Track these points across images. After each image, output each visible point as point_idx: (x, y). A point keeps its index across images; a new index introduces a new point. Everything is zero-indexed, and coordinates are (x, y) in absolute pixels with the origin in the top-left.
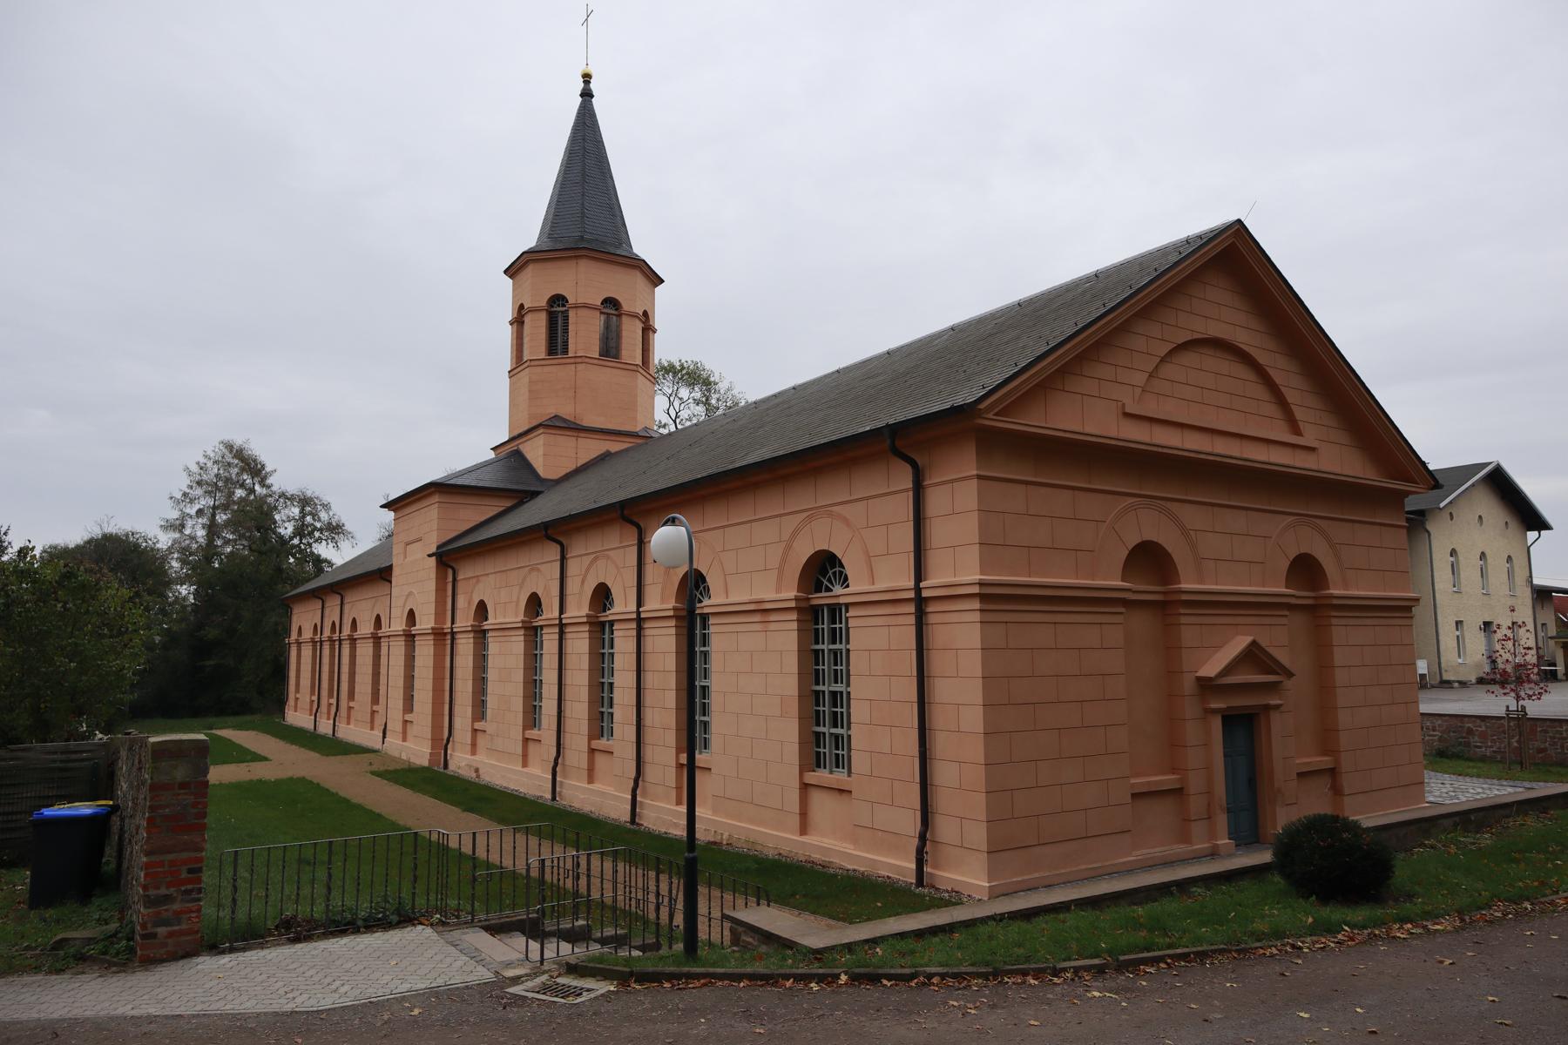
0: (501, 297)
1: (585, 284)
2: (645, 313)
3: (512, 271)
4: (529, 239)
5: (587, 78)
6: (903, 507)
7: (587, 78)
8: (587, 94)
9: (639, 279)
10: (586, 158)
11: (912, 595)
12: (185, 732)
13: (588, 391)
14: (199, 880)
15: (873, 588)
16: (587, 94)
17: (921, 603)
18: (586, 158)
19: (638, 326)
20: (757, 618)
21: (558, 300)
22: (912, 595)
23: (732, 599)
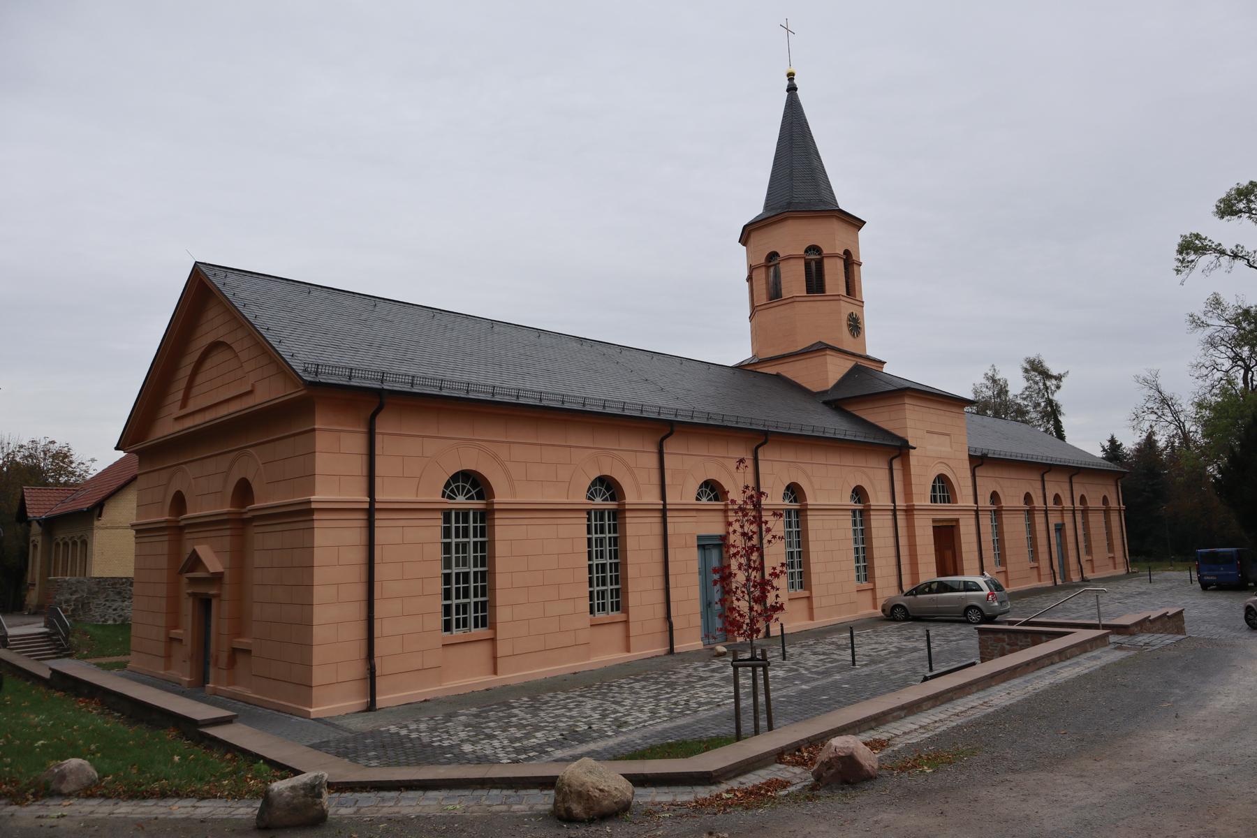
0: (738, 260)
1: (791, 239)
2: (847, 253)
3: (747, 235)
4: (755, 207)
5: (791, 76)
6: (652, 461)
7: (791, 76)
8: (792, 89)
9: (837, 227)
10: (795, 136)
11: (367, 506)
12: (1057, 688)
13: (811, 320)
14: (476, 626)
15: (566, 501)
16: (792, 89)
17: (977, 511)
18: (795, 136)
19: (840, 264)
20: (694, 514)
21: (773, 256)
22: (367, 506)
23: (684, 501)
